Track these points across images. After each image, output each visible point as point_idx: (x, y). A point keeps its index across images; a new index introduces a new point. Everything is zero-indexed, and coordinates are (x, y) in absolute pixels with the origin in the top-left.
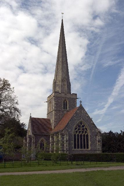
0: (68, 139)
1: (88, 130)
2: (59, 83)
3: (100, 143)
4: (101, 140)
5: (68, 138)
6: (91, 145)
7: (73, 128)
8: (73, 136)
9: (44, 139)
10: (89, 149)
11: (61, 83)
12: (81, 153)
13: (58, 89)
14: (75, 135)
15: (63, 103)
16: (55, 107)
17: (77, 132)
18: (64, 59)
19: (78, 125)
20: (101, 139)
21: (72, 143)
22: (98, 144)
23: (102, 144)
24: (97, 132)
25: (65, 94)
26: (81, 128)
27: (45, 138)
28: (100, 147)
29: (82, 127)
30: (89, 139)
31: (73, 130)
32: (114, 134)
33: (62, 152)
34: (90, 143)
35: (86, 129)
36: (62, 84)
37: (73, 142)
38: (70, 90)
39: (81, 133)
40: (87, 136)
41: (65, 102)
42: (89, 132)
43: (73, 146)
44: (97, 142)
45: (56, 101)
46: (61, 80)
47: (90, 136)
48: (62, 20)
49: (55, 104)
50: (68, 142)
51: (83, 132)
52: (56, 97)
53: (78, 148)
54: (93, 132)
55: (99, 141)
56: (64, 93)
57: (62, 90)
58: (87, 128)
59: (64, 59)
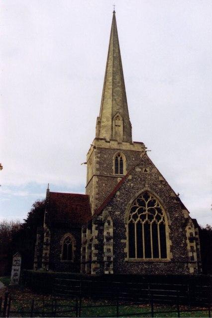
0: (112, 234)
1: (163, 211)
2: (107, 122)
3: (194, 244)
4: (197, 236)
5: (111, 230)
6: (172, 247)
8: (127, 226)
9: (71, 236)
11: (110, 123)
13: (106, 134)
14: (131, 225)
15: (114, 161)
16: (97, 170)
17: (135, 217)
18: (118, 78)
19: (139, 200)
20: (196, 233)
21: (125, 244)
22: (189, 248)
23: (199, 247)
24: (186, 217)
25: (119, 144)
27: (73, 234)
28: (195, 254)
30: (167, 234)
31: (127, 213)
32: (42, 203)
33: (98, 265)
34: (169, 243)
35: (159, 210)
36: (112, 124)
37: (127, 241)
38: (130, 135)
39: (147, 219)
40: (162, 226)
41: (119, 159)
42: (166, 218)
43: (126, 250)
44: (188, 241)
45: (99, 158)
47: (170, 227)
48: (114, 12)
50: (112, 241)
51: (151, 218)
52: (99, 148)
54: (176, 219)
55: (191, 240)
56: (116, 141)
57: (112, 135)
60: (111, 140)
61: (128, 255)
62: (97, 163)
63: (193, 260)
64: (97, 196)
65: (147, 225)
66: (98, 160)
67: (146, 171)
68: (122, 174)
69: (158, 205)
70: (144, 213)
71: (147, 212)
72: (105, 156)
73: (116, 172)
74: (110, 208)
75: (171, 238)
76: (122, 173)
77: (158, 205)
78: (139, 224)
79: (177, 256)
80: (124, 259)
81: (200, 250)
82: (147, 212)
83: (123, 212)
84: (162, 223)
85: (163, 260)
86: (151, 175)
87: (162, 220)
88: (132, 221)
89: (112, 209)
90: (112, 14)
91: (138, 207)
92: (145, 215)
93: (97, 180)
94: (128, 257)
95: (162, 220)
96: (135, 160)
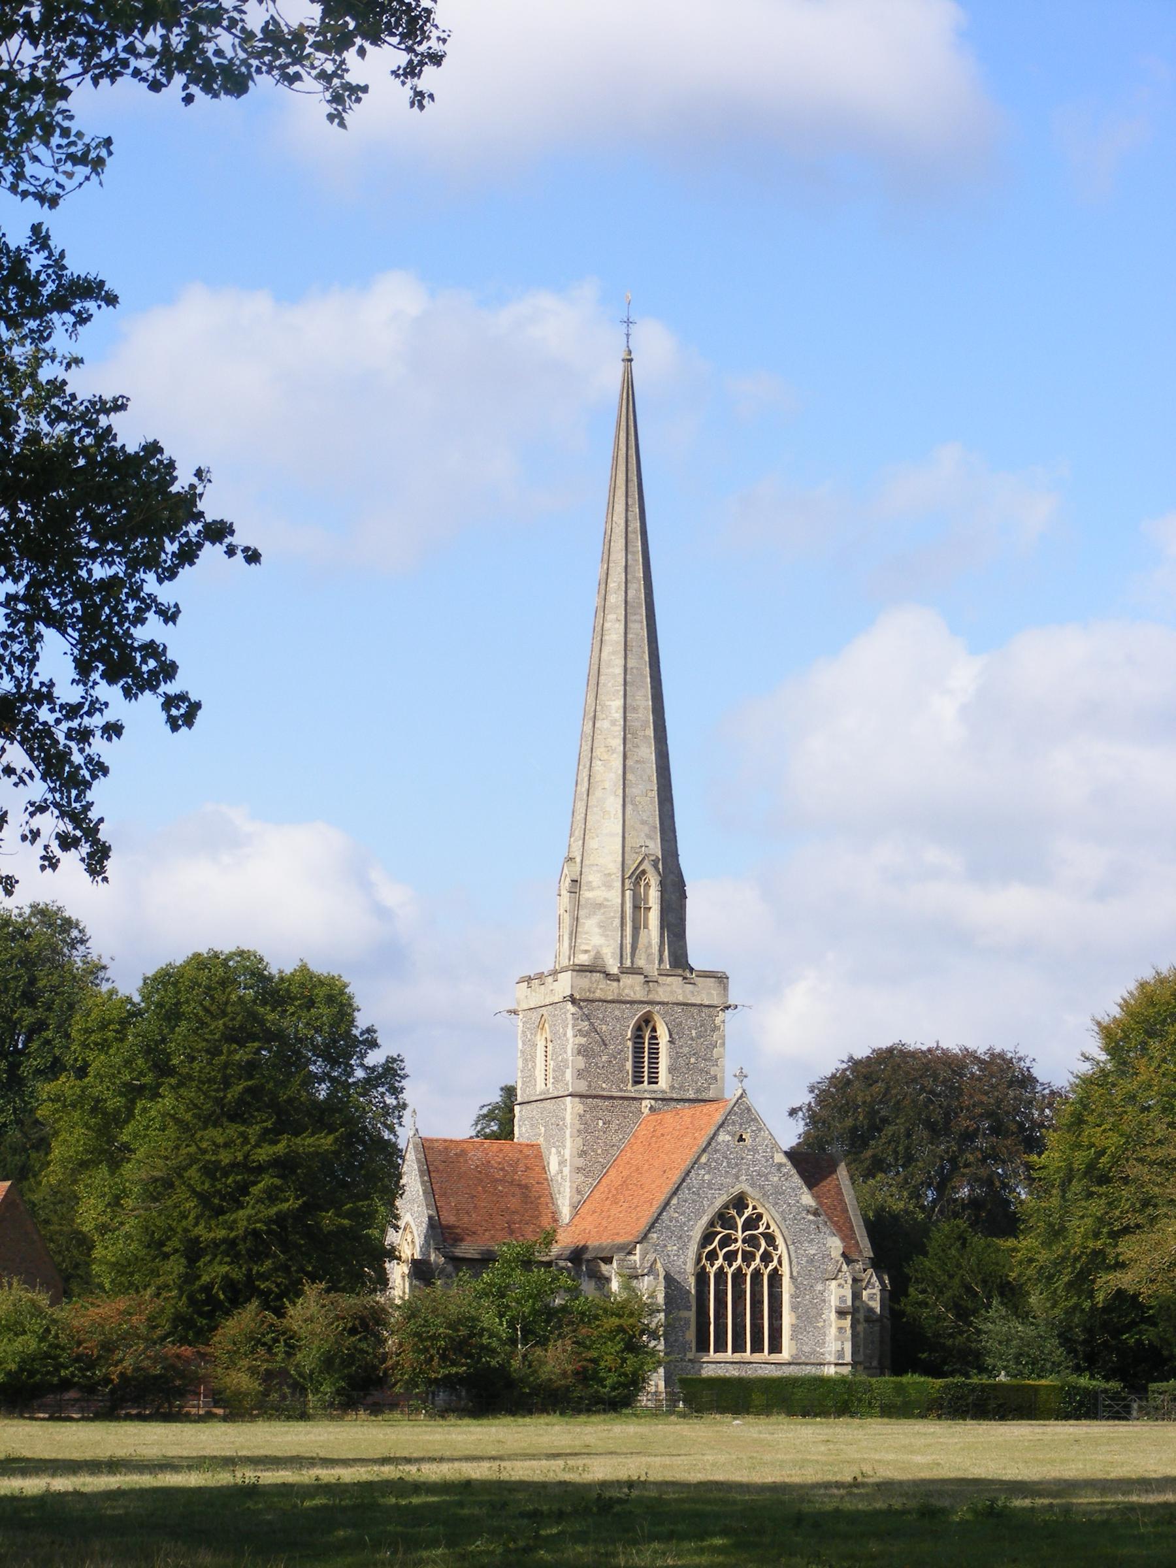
1: (780, 1241)
6: (795, 1328)
7: (690, 1238)
10: (785, 1355)
12: (733, 1372)
14: (702, 1277)
16: (580, 1074)
21: (688, 1321)
26: (740, 1235)
29: (746, 1227)
31: (693, 1247)
35: (770, 1239)
37: (692, 1315)
40: (775, 1277)
44: (833, 1316)
46: (614, 867)
49: (582, 1051)
51: (748, 1257)
53: (757, 1347)
54: (811, 1261)
58: (777, 1234)
59: (654, 645)
60: (624, 971)
61: (694, 1345)
62: (579, 1053)
63: (843, 1358)
64: (580, 1162)
65: (739, 1276)
66: (583, 1040)
67: (741, 1139)
68: (657, 1083)
69: (768, 1227)
70: (732, 1248)
71: (739, 1243)
72: (604, 1027)
73: (638, 1081)
74: (655, 1235)
75: (794, 1308)
76: (653, 1080)
77: (768, 1227)
78: (721, 1274)
79: (806, 1349)
80: (685, 1355)
81: (862, 1335)
82: (739, 1243)
83: (684, 1247)
84: (775, 1270)
85: (775, 1357)
86: (755, 1150)
87: (775, 1262)
88: (704, 1267)
89: (658, 1238)
90: (621, 366)
91: (720, 1233)
92: (736, 1252)
93: (580, 1108)
94: (694, 1349)
95: (775, 1262)
96: (699, 1036)
